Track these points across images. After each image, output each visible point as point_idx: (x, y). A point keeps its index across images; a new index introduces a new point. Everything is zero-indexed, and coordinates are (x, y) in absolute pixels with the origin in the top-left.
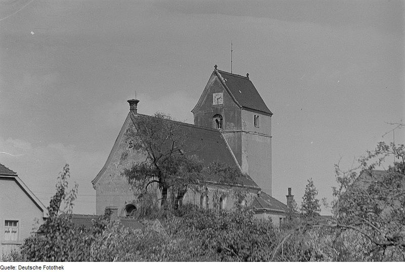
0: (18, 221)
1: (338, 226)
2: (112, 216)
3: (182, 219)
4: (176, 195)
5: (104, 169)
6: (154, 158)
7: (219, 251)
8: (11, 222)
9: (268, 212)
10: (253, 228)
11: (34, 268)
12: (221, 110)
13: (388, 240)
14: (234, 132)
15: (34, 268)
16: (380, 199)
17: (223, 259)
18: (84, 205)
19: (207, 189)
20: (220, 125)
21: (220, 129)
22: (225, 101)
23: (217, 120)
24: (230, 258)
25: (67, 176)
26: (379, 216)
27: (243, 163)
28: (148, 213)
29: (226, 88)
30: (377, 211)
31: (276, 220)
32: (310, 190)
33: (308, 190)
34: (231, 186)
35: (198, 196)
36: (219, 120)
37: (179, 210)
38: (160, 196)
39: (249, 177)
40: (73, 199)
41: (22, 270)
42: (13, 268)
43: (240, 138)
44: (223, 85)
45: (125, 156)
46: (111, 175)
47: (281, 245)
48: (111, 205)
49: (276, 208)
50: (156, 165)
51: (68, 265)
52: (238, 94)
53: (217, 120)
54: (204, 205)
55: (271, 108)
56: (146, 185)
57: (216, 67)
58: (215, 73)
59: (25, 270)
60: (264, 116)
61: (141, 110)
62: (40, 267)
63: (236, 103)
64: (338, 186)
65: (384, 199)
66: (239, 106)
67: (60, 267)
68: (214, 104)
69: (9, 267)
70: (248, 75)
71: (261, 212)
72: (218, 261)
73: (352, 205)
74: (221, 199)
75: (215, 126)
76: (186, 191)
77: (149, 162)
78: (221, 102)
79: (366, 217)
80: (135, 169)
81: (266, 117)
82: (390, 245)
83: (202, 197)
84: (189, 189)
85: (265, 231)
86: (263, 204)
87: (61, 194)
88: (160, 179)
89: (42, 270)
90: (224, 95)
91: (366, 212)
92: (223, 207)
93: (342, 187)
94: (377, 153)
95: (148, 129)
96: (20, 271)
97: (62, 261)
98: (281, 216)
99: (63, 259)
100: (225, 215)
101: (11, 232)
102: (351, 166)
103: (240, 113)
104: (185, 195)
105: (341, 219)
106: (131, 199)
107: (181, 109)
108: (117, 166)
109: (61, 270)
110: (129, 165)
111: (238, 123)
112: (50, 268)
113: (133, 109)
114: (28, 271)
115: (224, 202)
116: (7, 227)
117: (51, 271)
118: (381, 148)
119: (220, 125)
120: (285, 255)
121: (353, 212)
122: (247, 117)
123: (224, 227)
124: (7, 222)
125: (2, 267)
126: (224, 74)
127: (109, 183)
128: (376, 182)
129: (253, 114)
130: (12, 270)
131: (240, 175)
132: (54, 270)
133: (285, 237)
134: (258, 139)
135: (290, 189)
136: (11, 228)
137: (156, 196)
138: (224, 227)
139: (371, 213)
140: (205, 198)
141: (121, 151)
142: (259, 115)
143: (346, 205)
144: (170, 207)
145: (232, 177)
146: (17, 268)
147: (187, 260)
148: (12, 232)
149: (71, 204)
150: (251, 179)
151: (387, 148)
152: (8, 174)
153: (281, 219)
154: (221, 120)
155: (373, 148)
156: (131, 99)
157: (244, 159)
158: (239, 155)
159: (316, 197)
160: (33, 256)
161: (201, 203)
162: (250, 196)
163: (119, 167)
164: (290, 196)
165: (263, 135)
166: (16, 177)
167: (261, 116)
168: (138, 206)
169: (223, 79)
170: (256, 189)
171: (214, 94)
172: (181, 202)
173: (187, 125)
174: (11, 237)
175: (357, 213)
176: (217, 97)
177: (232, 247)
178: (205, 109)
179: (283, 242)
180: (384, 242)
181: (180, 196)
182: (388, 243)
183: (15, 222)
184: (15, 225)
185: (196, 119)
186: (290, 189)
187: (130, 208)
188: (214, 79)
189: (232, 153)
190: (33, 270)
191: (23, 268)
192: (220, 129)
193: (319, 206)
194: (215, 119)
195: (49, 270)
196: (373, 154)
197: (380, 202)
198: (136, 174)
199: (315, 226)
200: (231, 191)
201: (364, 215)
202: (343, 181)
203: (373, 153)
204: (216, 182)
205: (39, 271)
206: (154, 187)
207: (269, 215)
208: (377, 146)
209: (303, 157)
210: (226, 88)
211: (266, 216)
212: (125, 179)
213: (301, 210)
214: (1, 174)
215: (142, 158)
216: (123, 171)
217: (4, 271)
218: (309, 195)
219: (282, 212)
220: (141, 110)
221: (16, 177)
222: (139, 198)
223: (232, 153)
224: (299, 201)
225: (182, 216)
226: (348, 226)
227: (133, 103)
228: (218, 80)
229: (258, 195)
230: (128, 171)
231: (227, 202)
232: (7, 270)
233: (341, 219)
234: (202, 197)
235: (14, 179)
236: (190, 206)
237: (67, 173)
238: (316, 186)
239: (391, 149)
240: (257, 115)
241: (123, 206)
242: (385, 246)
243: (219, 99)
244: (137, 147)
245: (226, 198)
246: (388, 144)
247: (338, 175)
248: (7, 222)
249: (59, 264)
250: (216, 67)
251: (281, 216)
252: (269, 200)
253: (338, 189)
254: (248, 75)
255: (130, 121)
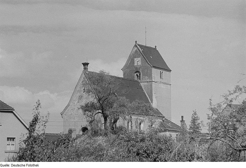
0: (15, 138)
1: (211, 138)
2: (73, 134)
3: (115, 135)
4: (113, 121)
5: (68, 105)
6: (98, 98)
7: (138, 154)
8: (11, 138)
9: (169, 131)
10: (159, 140)
11: (21, 166)
12: (140, 68)
13: (242, 147)
14: (148, 82)
15: (21, 166)
16: (237, 121)
17: (141, 160)
18: (54, 127)
19: (131, 117)
20: (139, 78)
21: (139, 80)
22: (142, 62)
23: (137, 75)
24: (145, 159)
25: (39, 108)
26: (236, 132)
27: (153, 101)
28: (96, 133)
29: (142, 55)
30: (235, 129)
31: (174, 135)
32: (194, 117)
33: (193, 117)
34: (147, 115)
35: (126, 122)
36: (138, 75)
37: (115, 131)
38: (103, 122)
39: (157, 110)
40: (46, 122)
41: (13, 167)
42: (8, 165)
43: (151, 86)
44: (141, 53)
45: (81, 97)
46: (72, 109)
47: (175, 151)
48: (72, 128)
49: (174, 128)
50: (100, 102)
51: (41, 164)
52: (150, 57)
53: (137, 75)
54: (130, 127)
55: (170, 67)
56: (94, 115)
57: (136, 42)
58: (136, 46)
59: (15, 167)
60: (157, 69)
61: (90, 69)
62: (24, 165)
63: (149, 64)
64: (210, 113)
65: (240, 121)
66: (150, 66)
67: (36, 165)
68: (135, 64)
69: (5, 165)
70: (156, 47)
71: (165, 131)
72: (137, 161)
73: (219, 125)
74: (140, 124)
75: (136, 78)
76: (118, 118)
77: (96, 101)
78: (140, 63)
79: (228, 132)
80: (87, 105)
81: (168, 73)
82: (243, 150)
83: (128, 122)
84: (120, 117)
85: (166, 142)
86: (166, 126)
87: (35, 120)
88: (102, 111)
89: (26, 167)
90: (141, 60)
91: (228, 129)
92: (142, 129)
93: (212, 114)
94: (235, 92)
95: (96, 81)
96: (12, 167)
97: (38, 161)
98: (177, 134)
99: (39, 160)
100: (143, 133)
101: (11, 145)
102: (218, 100)
103: (151, 71)
104: (118, 121)
105: (213, 134)
106: (85, 124)
107: (116, 69)
108: (76, 103)
109: (37, 167)
110: (83, 103)
111: (150, 76)
112: (30, 165)
113: (85, 69)
114: (17, 167)
115: (142, 125)
116: (8, 141)
117: (31, 167)
118: (237, 89)
119: (139, 78)
120: (180, 157)
121: (220, 129)
122: (155, 73)
123: (143, 140)
124: (8, 138)
125: (1, 165)
126: (141, 46)
127: (71, 114)
128: (234, 110)
129: (159, 71)
130: (8, 167)
131: (151, 108)
132: (32, 167)
133: (177, 146)
134: (162, 86)
135: (182, 117)
136: (11, 142)
137: (100, 121)
138: (143, 140)
139: (232, 130)
140: (130, 123)
141: (79, 94)
142: (163, 71)
143: (216, 125)
144: (109, 129)
145: (147, 111)
146: (10, 165)
147: (118, 161)
148: (12, 145)
149: (45, 126)
150: (158, 110)
151: (241, 89)
152: (8, 109)
153: (177, 135)
154: (140, 74)
155: (232, 89)
156: (84, 62)
157: (154, 99)
158: (151, 97)
159: (199, 121)
160: (21, 158)
161: (128, 126)
162: (158, 122)
163: (77, 104)
164: (182, 121)
165: (165, 84)
166: (13, 111)
167: (164, 72)
168: (89, 128)
169: (140, 49)
170: (161, 117)
171: (135, 59)
172: (116, 125)
173: (119, 78)
174: (12, 148)
175: (223, 130)
176: (137, 61)
177: (145, 152)
178: (130, 67)
179: (177, 149)
180: (240, 148)
181: (115, 122)
182: (242, 149)
183: (14, 139)
184: (13, 140)
185: (124, 74)
186: (182, 117)
187: (84, 129)
188: (135, 49)
189: (147, 95)
190: (20, 167)
191: (14, 165)
192: (139, 80)
193: (200, 127)
194: (136, 74)
195: (30, 167)
196: (232, 93)
197: (237, 123)
198: (87, 108)
199: (196, 138)
200: (146, 119)
201: (226, 132)
202: (213, 110)
203: (232, 92)
204: (137, 113)
205: (24, 167)
206: (99, 117)
207: (170, 133)
208: (235, 88)
209: (185, 96)
210: (142, 55)
211: (168, 134)
212: (81, 111)
213: (189, 129)
214: (1, 109)
215: (91, 99)
216: (80, 107)
217: (2, 167)
218: (194, 120)
219: (178, 131)
220: (90, 69)
221: (13, 111)
222: (90, 123)
223: (147, 95)
224: (188, 123)
225: (116, 134)
226: (217, 138)
227: (85, 65)
228: (138, 50)
229: (163, 120)
230: (82, 106)
231: (144, 125)
232: (4, 167)
233: (213, 134)
234: (128, 122)
235: (12, 112)
236: (121, 128)
237: (40, 106)
238: (199, 114)
239: (243, 90)
240: (162, 71)
241: (81, 128)
242: (240, 151)
243: (138, 62)
244: (89, 91)
245: (143, 123)
246: (241, 87)
247: (211, 106)
248: (8, 138)
249: (36, 163)
250: (136, 42)
251: (177, 134)
252: (170, 124)
253: (210, 116)
254: (156, 47)
255: (84, 76)
